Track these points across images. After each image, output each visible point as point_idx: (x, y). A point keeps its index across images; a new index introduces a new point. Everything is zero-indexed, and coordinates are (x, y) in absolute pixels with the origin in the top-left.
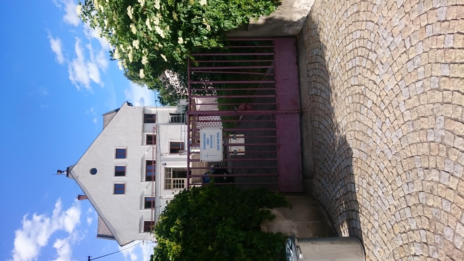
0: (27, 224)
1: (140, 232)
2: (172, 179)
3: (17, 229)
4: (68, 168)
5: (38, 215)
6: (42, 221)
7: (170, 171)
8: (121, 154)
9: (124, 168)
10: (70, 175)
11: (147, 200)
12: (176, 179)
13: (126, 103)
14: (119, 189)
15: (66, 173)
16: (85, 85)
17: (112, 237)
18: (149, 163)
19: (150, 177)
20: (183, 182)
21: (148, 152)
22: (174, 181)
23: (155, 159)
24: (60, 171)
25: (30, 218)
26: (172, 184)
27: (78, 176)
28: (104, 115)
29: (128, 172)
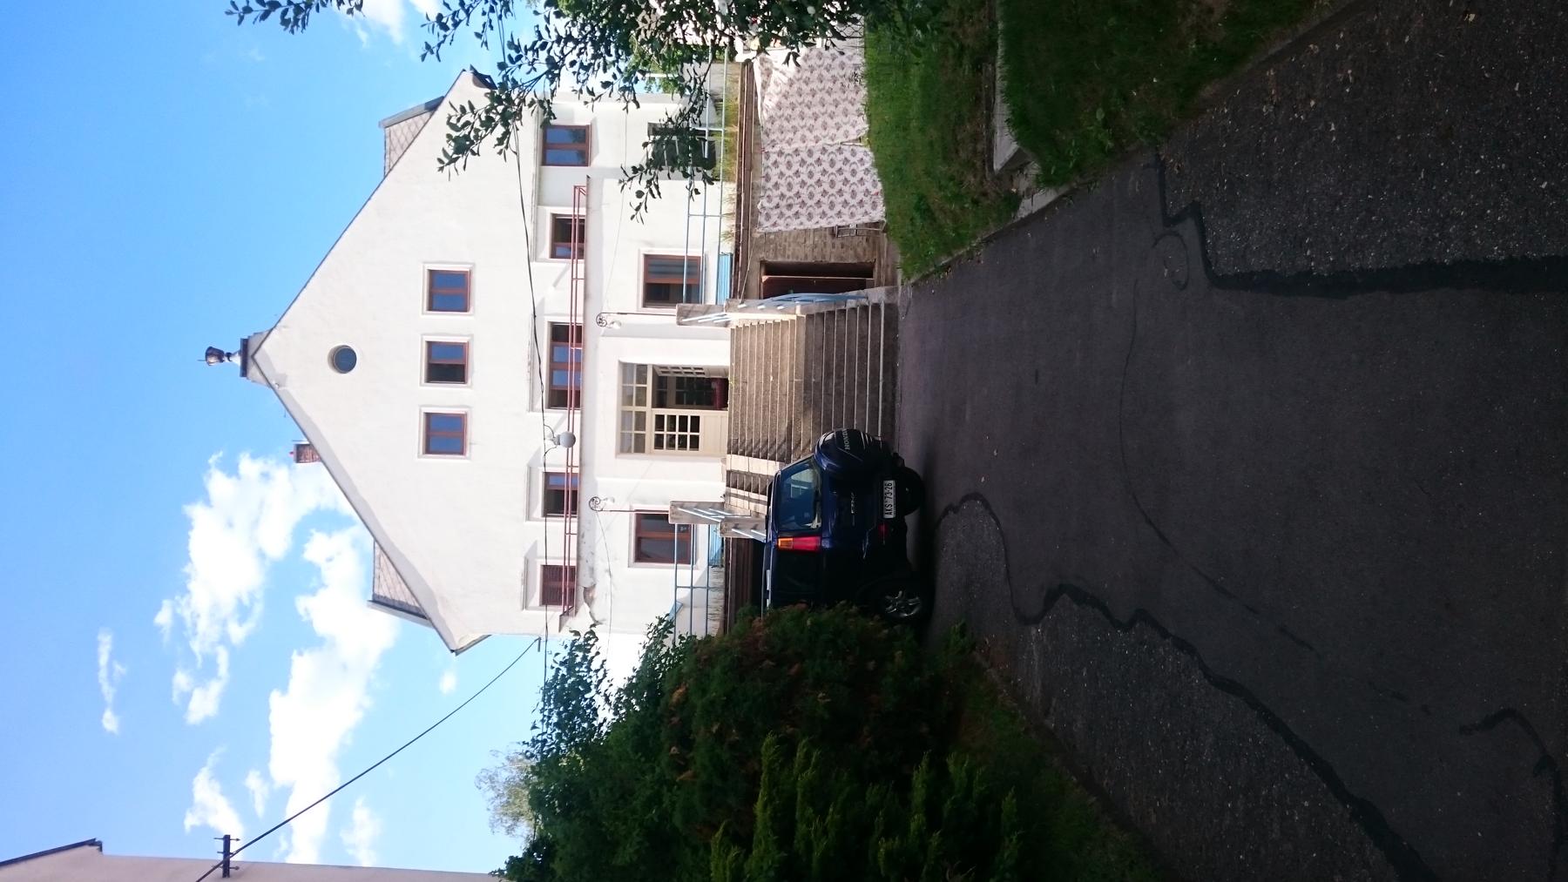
0: (218, 483)
1: (525, 606)
2: (651, 413)
3: (192, 500)
4: (245, 344)
5: (254, 457)
6: (265, 476)
7: (642, 378)
8: (448, 291)
9: (460, 349)
10: (253, 370)
11: (552, 481)
12: (666, 412)
13: (469, 75)
14: (444, 435)
15: (237, 360)
16: (387, 28)
17: (419, 614)
18: (560, 333)
19: (562, 396)
20: (695, 427)
21: (554, 289)
22: (660, 419)
23: (580, 320)
24: (216, 354)
25: (231, 469)
26: (650, 432)
27: (284, 377)
28: (388, 125)
29: (477, 365)
